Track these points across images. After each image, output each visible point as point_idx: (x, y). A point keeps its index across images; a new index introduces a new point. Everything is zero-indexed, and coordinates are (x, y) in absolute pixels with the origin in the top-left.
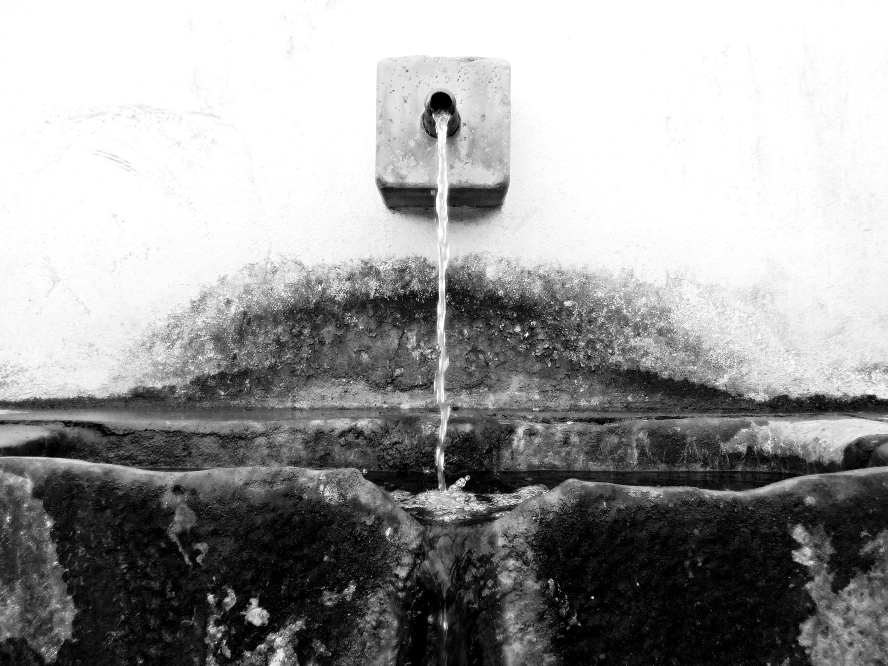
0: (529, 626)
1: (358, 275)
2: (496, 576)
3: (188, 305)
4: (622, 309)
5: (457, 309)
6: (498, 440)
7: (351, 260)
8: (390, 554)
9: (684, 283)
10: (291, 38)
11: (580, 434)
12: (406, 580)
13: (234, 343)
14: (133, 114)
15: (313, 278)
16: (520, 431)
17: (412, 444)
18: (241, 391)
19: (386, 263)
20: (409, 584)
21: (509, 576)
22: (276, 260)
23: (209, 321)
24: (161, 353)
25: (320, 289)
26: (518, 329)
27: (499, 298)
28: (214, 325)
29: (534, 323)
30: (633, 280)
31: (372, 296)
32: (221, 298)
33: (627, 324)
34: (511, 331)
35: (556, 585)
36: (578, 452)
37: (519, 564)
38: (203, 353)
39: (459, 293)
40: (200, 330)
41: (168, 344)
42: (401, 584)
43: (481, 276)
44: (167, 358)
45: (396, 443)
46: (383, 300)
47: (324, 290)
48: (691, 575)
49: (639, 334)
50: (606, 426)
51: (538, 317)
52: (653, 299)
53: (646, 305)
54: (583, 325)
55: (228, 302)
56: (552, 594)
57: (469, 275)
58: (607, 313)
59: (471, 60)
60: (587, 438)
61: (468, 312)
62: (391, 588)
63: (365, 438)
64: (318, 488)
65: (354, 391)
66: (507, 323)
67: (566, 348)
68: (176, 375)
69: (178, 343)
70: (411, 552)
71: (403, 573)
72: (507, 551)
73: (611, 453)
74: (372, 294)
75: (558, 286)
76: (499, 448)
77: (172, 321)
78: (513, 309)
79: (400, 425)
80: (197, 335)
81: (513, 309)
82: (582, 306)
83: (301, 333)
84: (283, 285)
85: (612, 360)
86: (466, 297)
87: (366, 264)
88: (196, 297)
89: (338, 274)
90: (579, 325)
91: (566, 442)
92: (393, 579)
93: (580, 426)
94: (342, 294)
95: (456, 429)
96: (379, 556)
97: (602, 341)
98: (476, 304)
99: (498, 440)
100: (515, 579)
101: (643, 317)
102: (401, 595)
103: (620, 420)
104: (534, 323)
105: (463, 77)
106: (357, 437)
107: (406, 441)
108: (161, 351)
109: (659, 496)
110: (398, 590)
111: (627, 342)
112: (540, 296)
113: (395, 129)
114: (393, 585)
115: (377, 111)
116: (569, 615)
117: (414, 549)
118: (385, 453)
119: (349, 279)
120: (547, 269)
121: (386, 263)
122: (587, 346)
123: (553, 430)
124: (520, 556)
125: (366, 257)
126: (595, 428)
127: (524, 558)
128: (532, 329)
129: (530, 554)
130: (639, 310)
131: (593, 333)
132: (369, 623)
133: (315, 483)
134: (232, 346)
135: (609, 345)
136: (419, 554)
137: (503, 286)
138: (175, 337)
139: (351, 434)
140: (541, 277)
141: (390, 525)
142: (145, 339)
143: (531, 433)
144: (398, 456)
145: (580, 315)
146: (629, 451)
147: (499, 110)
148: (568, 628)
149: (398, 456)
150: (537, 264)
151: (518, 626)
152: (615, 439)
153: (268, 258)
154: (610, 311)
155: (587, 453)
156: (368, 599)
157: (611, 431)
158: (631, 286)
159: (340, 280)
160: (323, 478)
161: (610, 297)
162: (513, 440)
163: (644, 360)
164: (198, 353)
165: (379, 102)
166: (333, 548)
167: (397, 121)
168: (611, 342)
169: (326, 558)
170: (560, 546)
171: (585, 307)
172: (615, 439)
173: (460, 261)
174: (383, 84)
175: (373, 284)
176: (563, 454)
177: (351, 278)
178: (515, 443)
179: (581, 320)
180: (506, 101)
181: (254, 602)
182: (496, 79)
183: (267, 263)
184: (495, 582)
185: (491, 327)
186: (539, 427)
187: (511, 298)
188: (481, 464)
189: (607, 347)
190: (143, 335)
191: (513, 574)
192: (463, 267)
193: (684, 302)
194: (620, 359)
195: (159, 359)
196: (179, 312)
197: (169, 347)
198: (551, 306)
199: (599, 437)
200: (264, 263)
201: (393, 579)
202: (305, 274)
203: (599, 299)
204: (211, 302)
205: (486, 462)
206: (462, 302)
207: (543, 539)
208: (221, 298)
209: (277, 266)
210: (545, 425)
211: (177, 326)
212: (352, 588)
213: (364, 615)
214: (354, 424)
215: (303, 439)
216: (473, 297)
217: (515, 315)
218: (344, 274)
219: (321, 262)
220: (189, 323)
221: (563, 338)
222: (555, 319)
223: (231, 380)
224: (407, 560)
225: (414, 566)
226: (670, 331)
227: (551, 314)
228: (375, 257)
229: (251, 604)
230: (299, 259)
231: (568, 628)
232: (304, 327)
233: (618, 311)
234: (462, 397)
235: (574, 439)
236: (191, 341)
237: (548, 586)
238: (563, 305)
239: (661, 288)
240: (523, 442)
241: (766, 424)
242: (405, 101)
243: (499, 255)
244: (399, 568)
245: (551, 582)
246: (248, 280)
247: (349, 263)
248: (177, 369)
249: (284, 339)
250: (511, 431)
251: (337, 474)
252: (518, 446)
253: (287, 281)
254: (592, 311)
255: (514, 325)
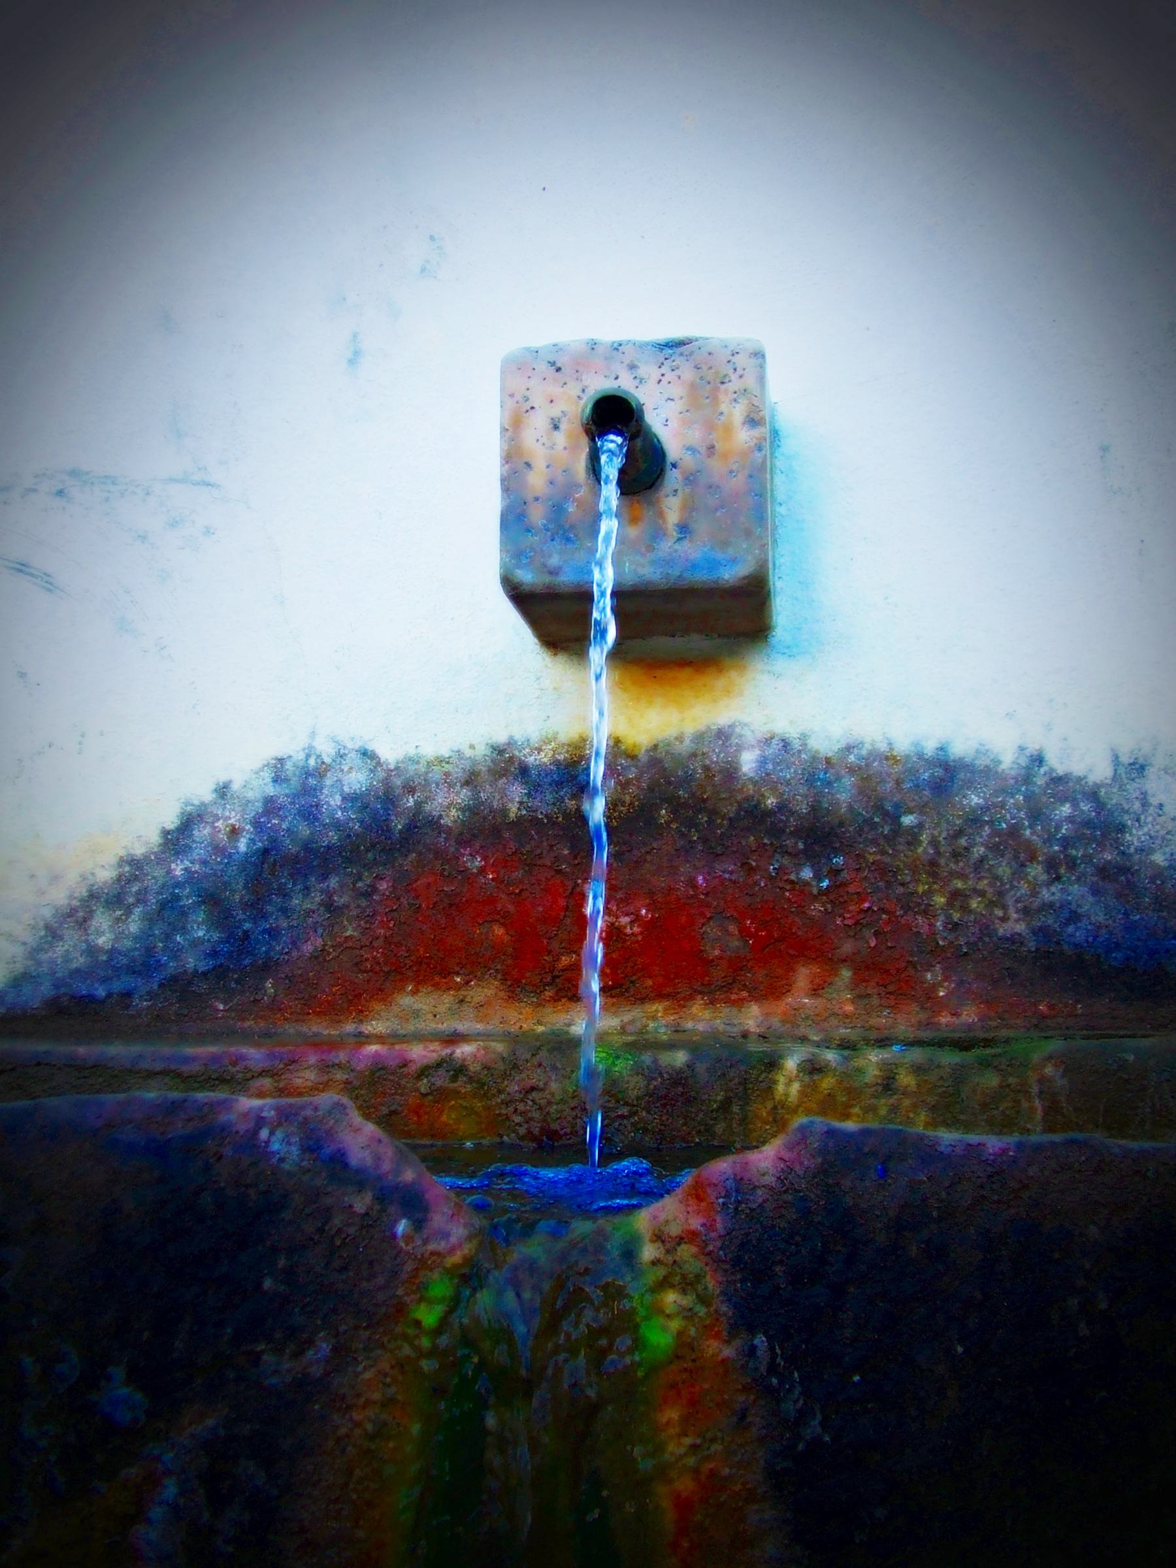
0: (713, 1440)
1: (485, 776)
2: (637, 1327)
3: (155, 839)
4: (1022, 827)
5: (683, 835)
6: (744, 1082)
7: (472, 747)
8: (404, 1276)
9: (1151, 772)
10: (355, 336)
11: (917, 1069)
12: (438, 1331)
13: (244, 911)
14: (60, 487)
15: (398, 782)
16: (791, 1064)
17: (565, 1091)
18: (256, 1001)
19: (539, 750)
20: (444, 1340)
21: (665, 1329)
22: (326, 750)
23: (197, 867)
24: (104, 932)
25: (411, 802)
26: (807, 874)
27: (769, 813)
28: (206, 876)
29: (839, 860)
30: (1042, 770)
31: (512, 815)
32: (219, 824)
33: (1032, 858)
34: (793, 877)
35: (772, 1349)
36: (915, 1106)
37: (687, 1301)
38: (184, 930)
39: (685, 805)
40: (177, 885)
41: (119, 913)
42: (425, 1342)
43: (730, 773)
44: (116, 939)
45: (533, 1089)
46: (535, 821)
47: (418, 804)
48: (1083, 1330)
49: (1058, 878)
50: (976, 1052)
51: (845, 848)
52: (1085, 807)
53: (1070, 819)
54: (942, 862)
55: (234, 832)
56: (763, 1369)
57: (706, 768)
58: (990, 836)
59: (681, 343)
60: (932, 1077)
61: (705, 841)
62: (407, 1350)
63: (471, 1079)
64: (255, 1132)
65: (476, 1000)
66: (786, 861)
67: (907, 909)
68: (131, 970)
69: (138, 911)
70: (450, 1272)
71: (429, 1317)
72: (661, 1272)
73: (984, 1106)
74: (513, 810)
75: (889, 786)
76: (745, 1099)
77: (127, 869)
78: (796, 833)
79: (543, 1053)
80: (173, 894)
81: (796, 833)
82: (938, 825)
83: (374, 889)
84: (338, 798)
85: (1002, 930)
86: (700, 811)
87: (501, 752)
88: (171, 820)
89: (447, 774)
90: (933, 863)
91: (888, 1084)
92: (411, 1331)
93: (916, 1055)
94: (453, 812)
95: (655, 1061)
96: (380, 1280)
97: (982, 894)
98: (721, 826)
99: (744, 1082)
100: (680, 1334)
101: (1066, 843)
102: (426, 1365)
103: (1007, 1041)
104: (839, 860)
105: (671, 376)
106: (454, 1078)
107: (554, 1086)
108: (105, 926)
109: (1004, 1151)
110: (421, 1354)
111: (1034, 893)
112: (850, 807)
113: (537, 481)
114: (411, 1344)
115: (502, 449)
116: (803, 1416)
117: (456, 1266)
118: (511, 1109)
119: (467, 783)
120: (864, 752)
121: (539, 750)
122: (950, 904)
123: (860, 1062)
124: (687, 1284)
125: (501, 738)
126: (949, 1058)
127: (700, 1287)
128: (835, 872)
129: (711, 1283)
130: (1058, 828)
131: (962, 876)
132: (358, 1424)
133: (252, 1125)
134: (241, 916)
135: (998, 901)
136: (469, 1277)
137: (774, 789)
138: (131, 900)
139: (441, 1072)
140: (852, 770)
141: (404, 1216)
142: (75, 903)
143: (813, 1068)
144: (536, 1115)
145: (934, 842)
146: (1025, 1104)
147: (744, 436)
148: (801, 1447)
149: (536, 1115)
150: (842, 744)
151: (688, 1441)
152: (991, 1080)
153: (311, 747)
154: (996, 833)
155: (933, 1109)
156: (357, 1375)
157: (985, 1064)
158: (1040, 781)
159: (451, 786)
160: (269, 1114)
161: (995, 805)
162: (775, 1082)
163: (1070, 929)
164: (175, 930)
165: (504, 430)
166: (282, 1262)
167: (540, 464)
168: (1001, 894)
169: (267, 1283)
170: (781, 1262)
171: (944, 825)
172: (991, 1080)
173: (687, 742)
174: (512, 396)
175: (517, 792)
176: (883, 1111)
177: (471, 780)
178: (780, 1088)
179: (938, 853)
180: (756, 418)
181: (118, 1372)
182: (733, 377)
183: (308, 756)
184: (635, 1340)
185: (752, 870)
186: (831, 1056)
187: (792, 813)
188: (709, 1130)
189: (991, 904)
190: (71, 897)
191: (675, 1325)
192: (694, 755)
193: (1151, 810)
194: (1020, 927)
195: (101, 941)
196: (139, 851)
197: (118, 919)
198: (874, 826)
199: (959, 1075)
200: (302, 756)
201: (411, 1331)
202: (381, 774)
203: (973, 810)
204: (202, 833)
205: (719, 1128)
206: (692, 824)
207: (742, 1245)
208: (219, 824)
209: (328, 760)
210: (846, 1053)
211: (136, 878)
212: (324, 1346)
213: (349, 1408)
214: (448, 1051)
215: (347, 1082)
216: (713, 813)
217: (801, 846)
218: (457, 772)
219: (412, 752)
220: (159, 872)
221: (900, 890)
222: (883, 852)
223: (237, 982)
224: (440, 1288)
225: (454, 1304)
226: (1124, 870)
227: (874, 842)
228: (519, 737)
229: (109, 1378)
230: (370, 747)
231: (801, 1447)
232: (379, 878)
233: (1014, 832)
234: (694, 1010)
235: (906, 1079)
236: (163, 906)
237: (753, 1349)
238: (900, 824)
239: (1102, 785)
240: (795, 1087)
241: (607, 477)
242: (556, 427)
243: (765, 729)
244: (423, 1306)
245: (760, 1340)
246: (271, 790)
247: (468, 753)
248: (134, 961)
249: (339, 900)
250: (772, 1064)
251: (303, 1107)
252: (787, 1095)
253: (346, 789)
254: (959, 833)
255: (799, 867)
